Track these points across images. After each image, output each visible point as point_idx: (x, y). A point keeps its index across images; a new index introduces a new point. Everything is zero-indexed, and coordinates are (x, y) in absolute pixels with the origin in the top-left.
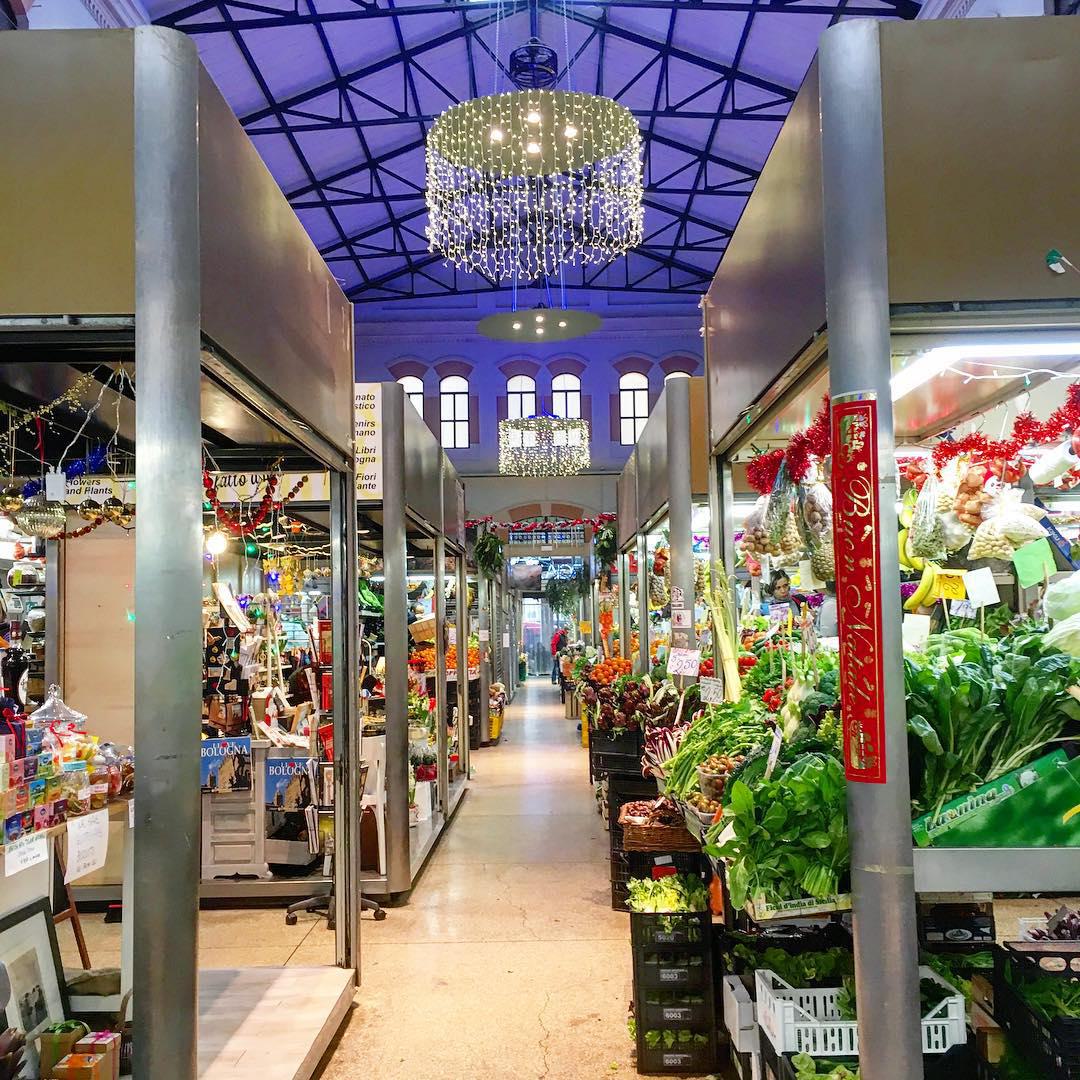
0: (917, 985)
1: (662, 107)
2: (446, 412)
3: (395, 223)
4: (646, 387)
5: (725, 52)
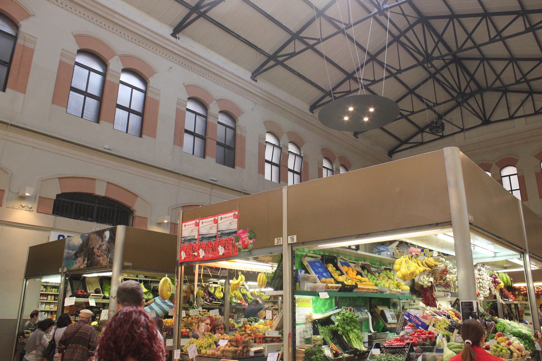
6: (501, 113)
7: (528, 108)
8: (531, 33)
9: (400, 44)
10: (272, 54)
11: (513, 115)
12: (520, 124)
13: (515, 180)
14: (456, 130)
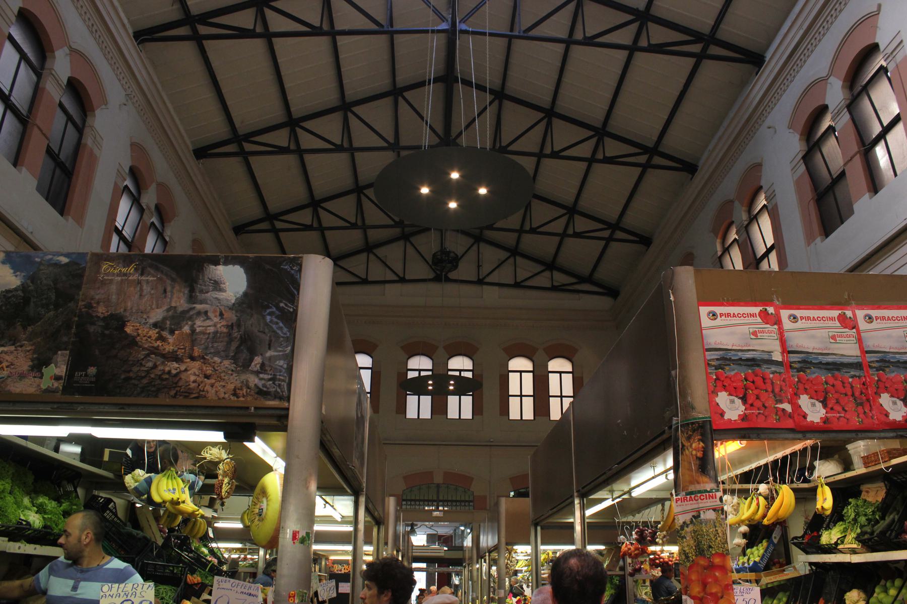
1: (527, 227)
2: (554, 389)
4: (532, 369)
5: (567, 193)
6: (465, 270)
10: (196, 13)
11: (485, 278)
12: (491, 295)
13: (568, 379)
14: (390, 276)
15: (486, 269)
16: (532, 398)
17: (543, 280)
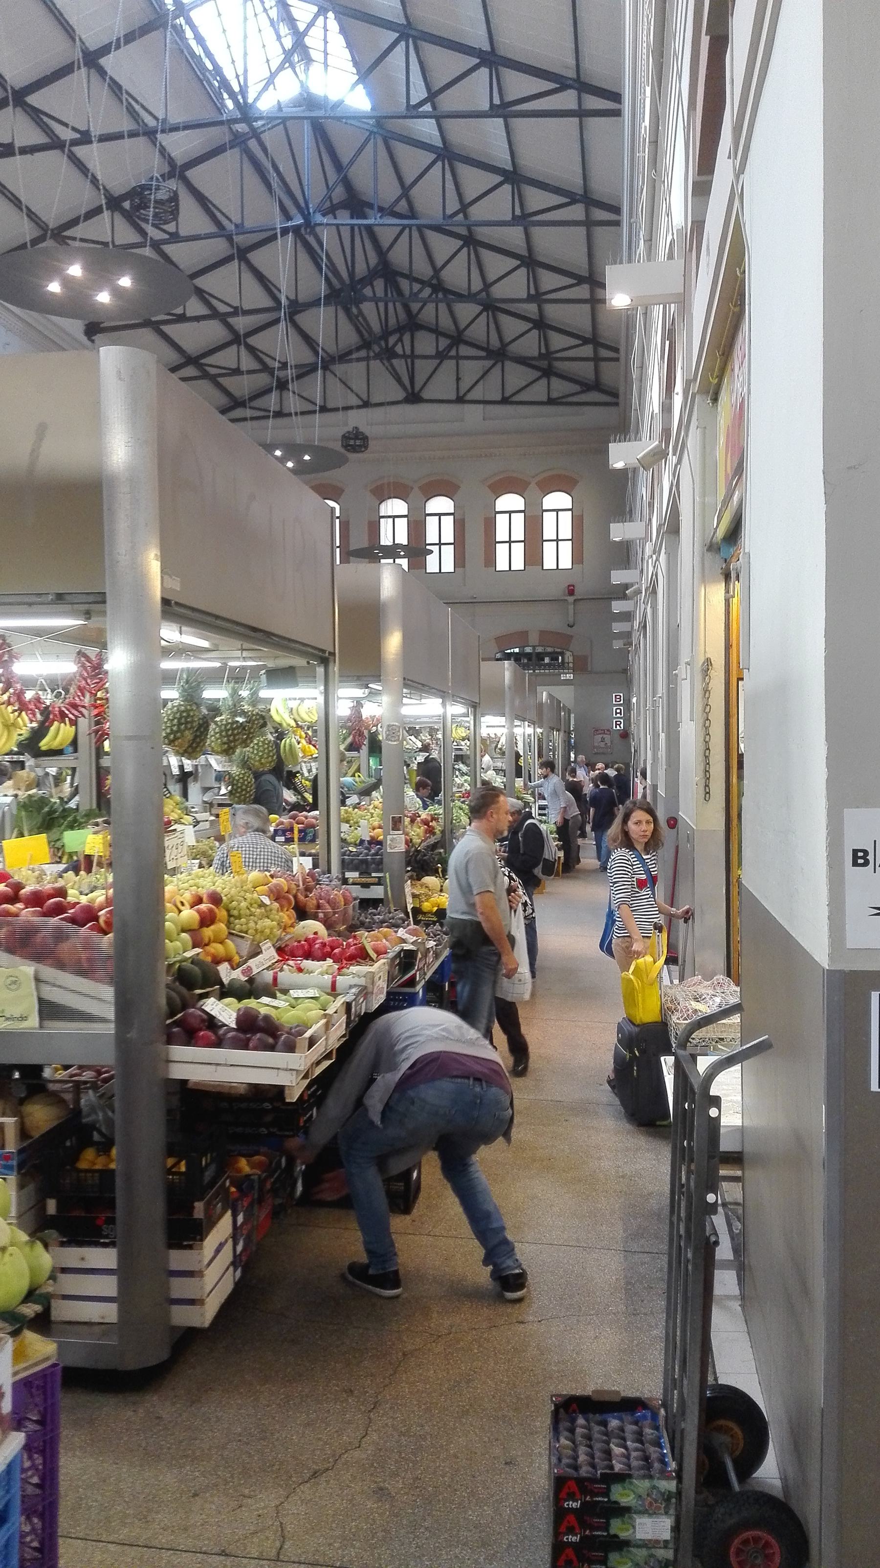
0: (403, 1283)
2: (549, 532)
3: (596, 359)
7: (491, 389)
8: (520, 229)
9: (301, 241)
11: (465, 394)
12: (473, 414)
13: (448, 523)
14: (355, 401)
15: (465, 386)
16: (523, 544)
17: (539, 391)
